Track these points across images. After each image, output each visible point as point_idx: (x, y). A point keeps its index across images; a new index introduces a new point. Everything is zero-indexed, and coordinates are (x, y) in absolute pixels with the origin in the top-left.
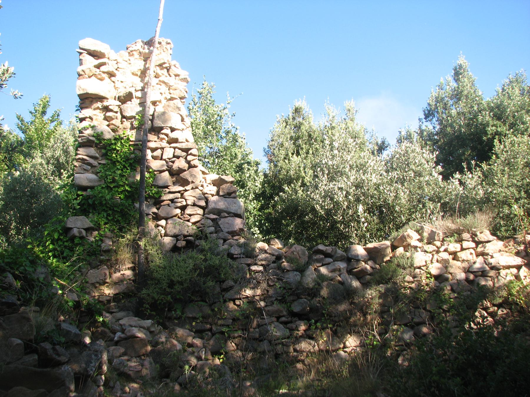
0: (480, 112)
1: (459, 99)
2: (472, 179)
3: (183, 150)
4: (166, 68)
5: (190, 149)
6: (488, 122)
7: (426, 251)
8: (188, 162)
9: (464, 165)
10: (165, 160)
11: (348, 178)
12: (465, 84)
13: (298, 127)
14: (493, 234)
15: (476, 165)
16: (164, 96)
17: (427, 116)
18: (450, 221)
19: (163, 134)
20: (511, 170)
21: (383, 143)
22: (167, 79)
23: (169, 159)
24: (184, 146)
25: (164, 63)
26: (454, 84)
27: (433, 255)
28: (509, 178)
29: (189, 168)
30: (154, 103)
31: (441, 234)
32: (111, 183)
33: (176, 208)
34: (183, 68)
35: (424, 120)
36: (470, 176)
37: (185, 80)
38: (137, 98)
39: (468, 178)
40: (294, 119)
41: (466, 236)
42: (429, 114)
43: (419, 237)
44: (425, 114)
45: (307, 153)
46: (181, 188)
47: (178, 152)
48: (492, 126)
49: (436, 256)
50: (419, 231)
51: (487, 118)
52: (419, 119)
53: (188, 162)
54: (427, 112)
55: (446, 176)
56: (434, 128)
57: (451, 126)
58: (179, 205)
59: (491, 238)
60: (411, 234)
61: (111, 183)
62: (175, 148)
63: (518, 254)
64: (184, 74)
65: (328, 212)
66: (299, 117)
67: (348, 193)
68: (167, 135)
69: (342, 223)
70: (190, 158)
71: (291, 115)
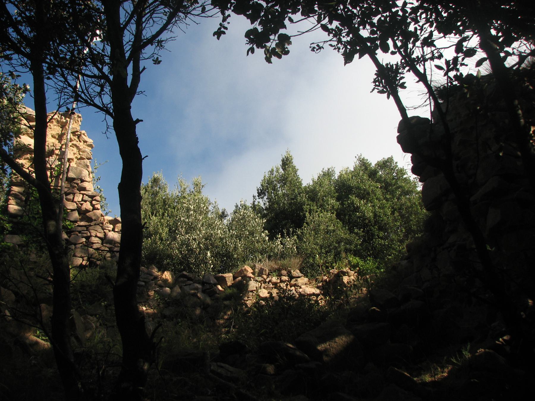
0: (299, 194)
1: (285, 184)
2: (290, 242)
3: (89, 196)
4: (77, 135)
5: (96, 196)
6: (304, 201)
7: (256, 281)
8: (93, 206)
9: (285, 231)
10: (75, 202)
11: (200, 231)
12: (290, 173)
13: (155, 194)
14: (301, 272)
15: (293, 232)
16: (76, 155)
17: (259, 194)
18: (273, 262)
19: (75, 183)
20: (316, 234)
21: (223, 213)
22: (78, 144)
23: (79, 202)
24: (90, 193)
25: (77, 131)
26: (281, 171)
27: (261, 284)
28: (314, 239)
29: (93, 210)
30: (69, 160)
31: (267, 271)
32: (36, 214)
33: (83, 237)
34: (89, 137)
35: (257, 197)
36: (289, 239)
37: (90, 146)
38: (57, 155)
39: (287, 241)
40: (152, 187)
41: (284, 272)
42: (261, 193)
43: (252, 271)
44: (258, 193)
45: (163, 215)
46: (87, 224)
47: (86, 198)
48: (307, 205)
49: (263, 285)
50: (253, 268)
51: (304, 199)
52: (253, 196)
53: (93, 206)
54: (260, 191)
55: (272, 237)
56: (264, 204)
57: (278, 204)
58: (85, 235)
59: (300, 275)
60: (247, 269)
61: (36, 214)
62: (83, 194)
63: (318, 287)
64: (90, 141)
65: (185, 257)
66: (156, 186)
67: (199, 243)
68: (78, 184)
69: (194, 264)
70: (94, 202)
71: (150, 184)
